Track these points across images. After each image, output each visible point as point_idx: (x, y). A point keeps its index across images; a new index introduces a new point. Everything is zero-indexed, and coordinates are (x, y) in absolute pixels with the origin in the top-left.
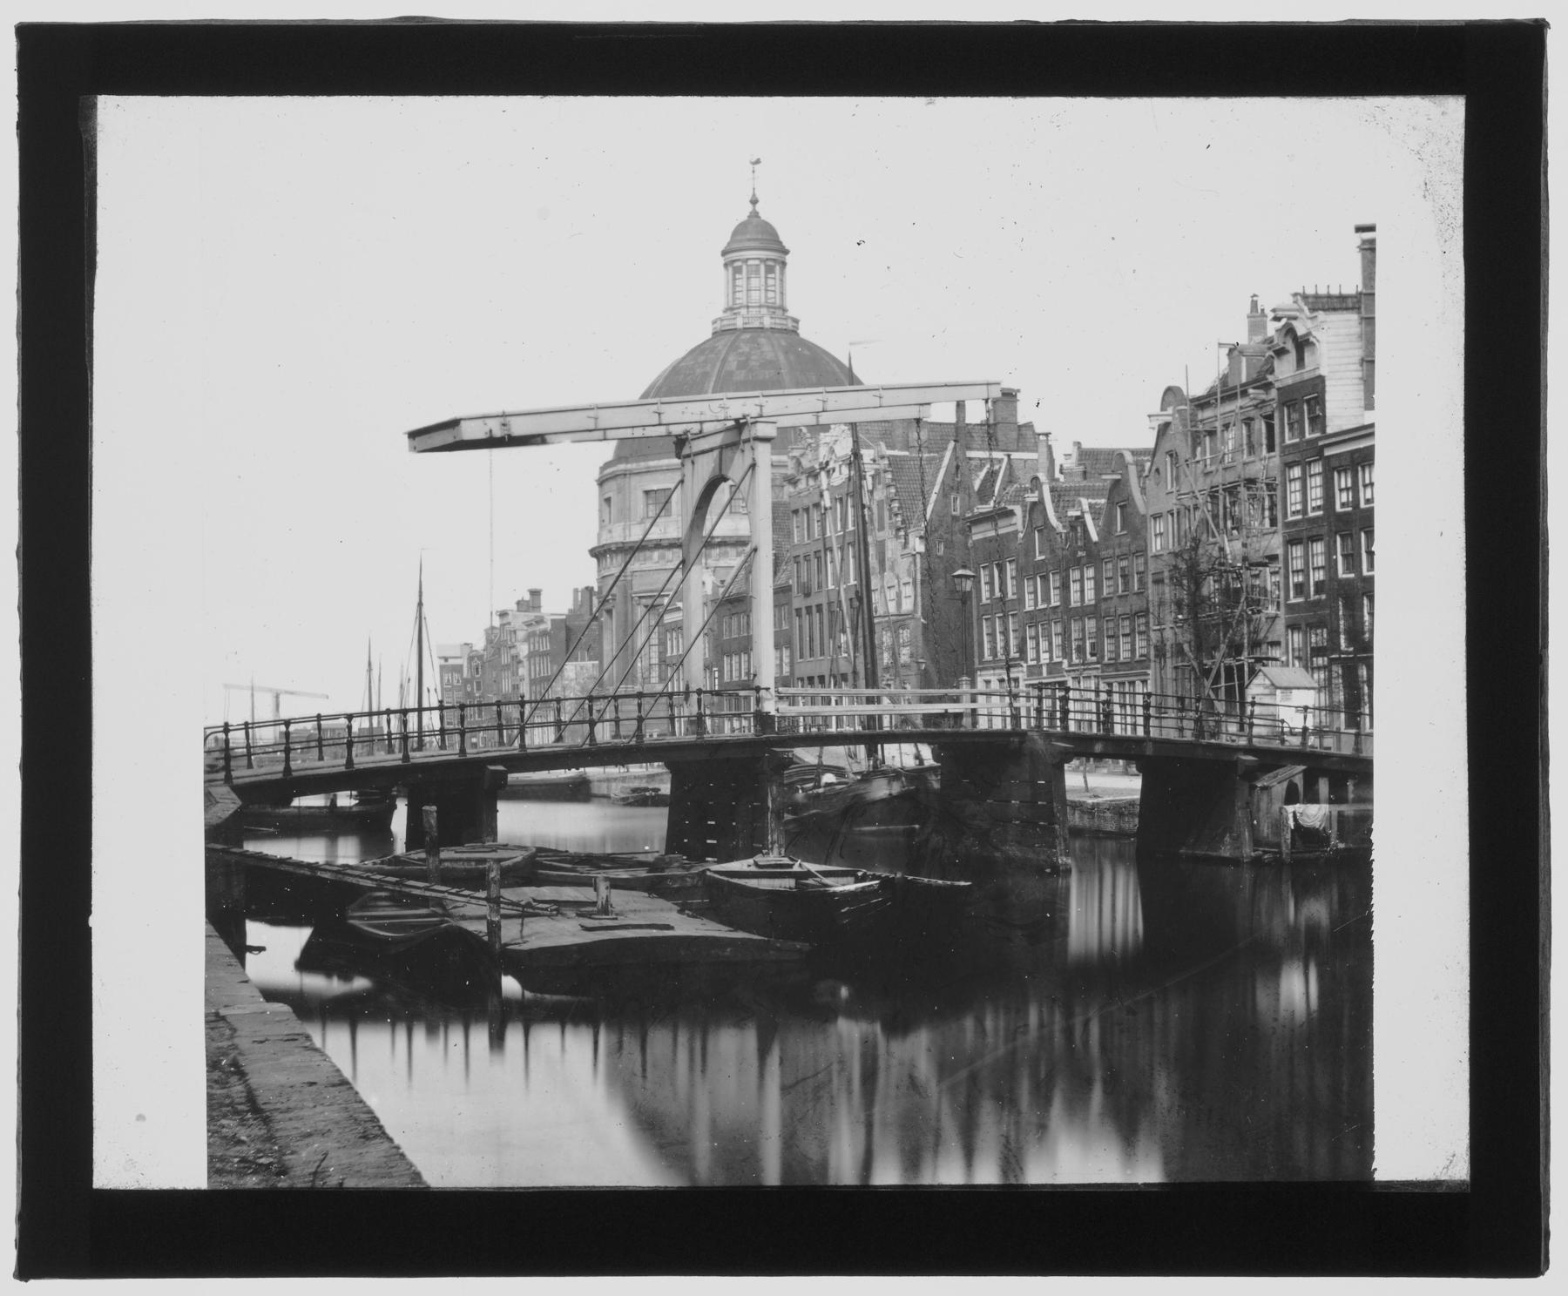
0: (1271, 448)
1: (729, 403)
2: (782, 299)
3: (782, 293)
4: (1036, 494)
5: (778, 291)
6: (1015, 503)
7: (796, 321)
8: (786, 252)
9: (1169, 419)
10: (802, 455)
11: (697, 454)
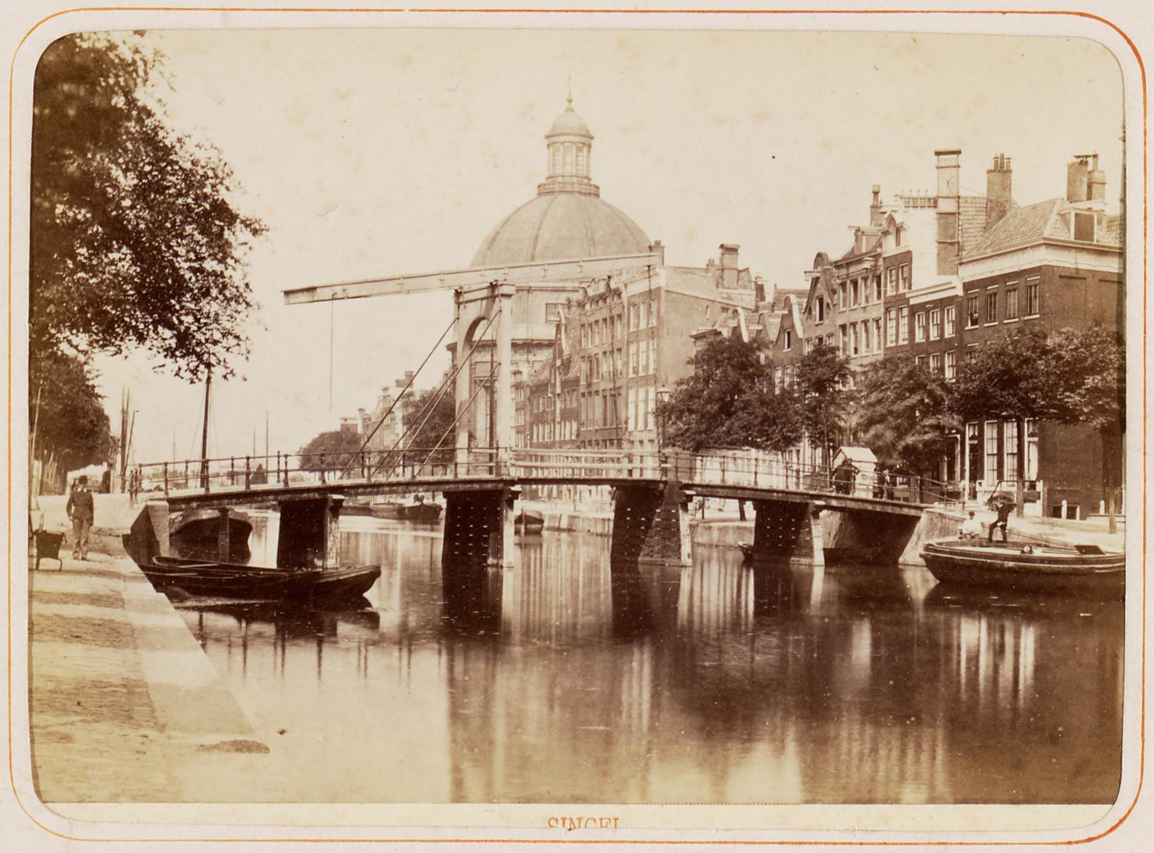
0: (879, 297)
1: (486, 273)
2: (588, 172)
3: (588, 167)
4: (736, 321)
5: (585, 167)
6: (724, 326)
7: (597, 187)
8: (592, 138)
9: (818, 275)
10: (589, 286)
11: (466, 302)
